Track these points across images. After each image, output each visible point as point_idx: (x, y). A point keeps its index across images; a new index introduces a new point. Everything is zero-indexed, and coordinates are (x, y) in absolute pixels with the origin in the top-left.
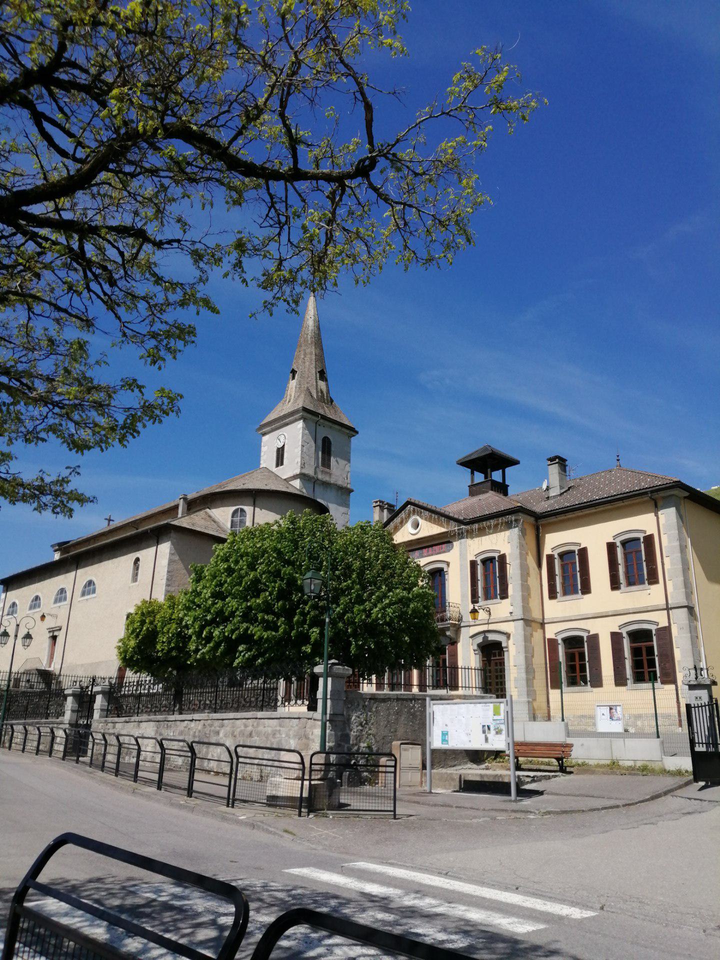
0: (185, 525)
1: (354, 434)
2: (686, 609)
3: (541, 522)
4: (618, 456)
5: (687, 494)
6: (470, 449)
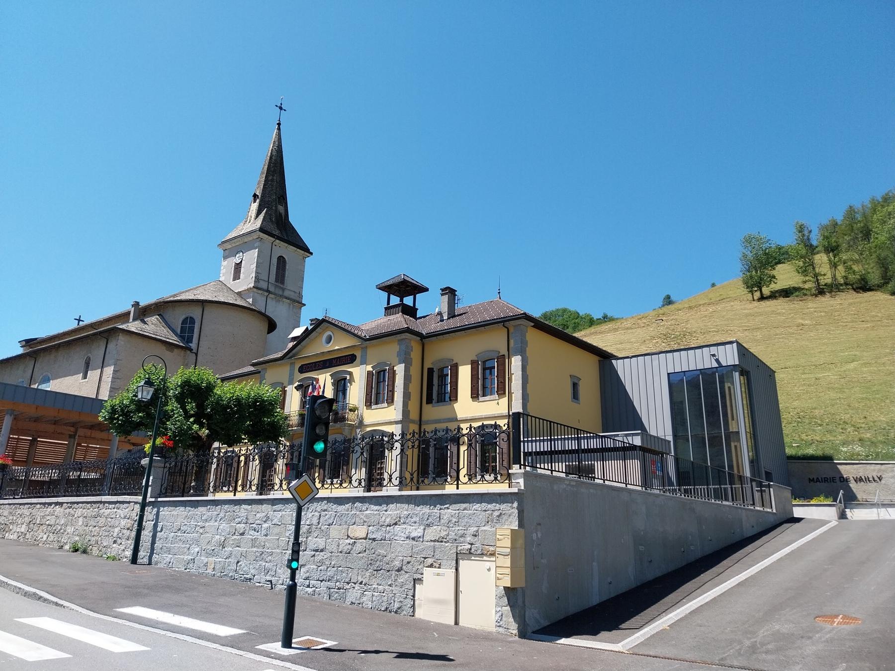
0: (133, 329)
1: (308, 255)
2: (462, 563)
3: (425, 341)
4: (499, 290)
5: (533, 324)
6: (390, 275)
